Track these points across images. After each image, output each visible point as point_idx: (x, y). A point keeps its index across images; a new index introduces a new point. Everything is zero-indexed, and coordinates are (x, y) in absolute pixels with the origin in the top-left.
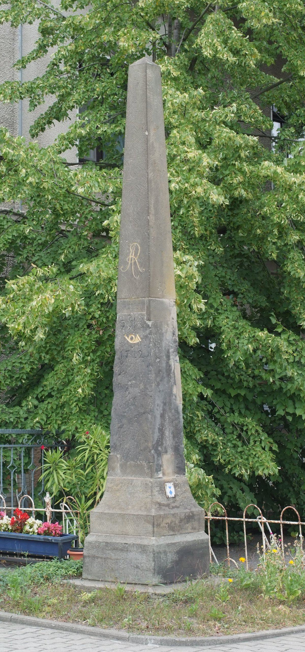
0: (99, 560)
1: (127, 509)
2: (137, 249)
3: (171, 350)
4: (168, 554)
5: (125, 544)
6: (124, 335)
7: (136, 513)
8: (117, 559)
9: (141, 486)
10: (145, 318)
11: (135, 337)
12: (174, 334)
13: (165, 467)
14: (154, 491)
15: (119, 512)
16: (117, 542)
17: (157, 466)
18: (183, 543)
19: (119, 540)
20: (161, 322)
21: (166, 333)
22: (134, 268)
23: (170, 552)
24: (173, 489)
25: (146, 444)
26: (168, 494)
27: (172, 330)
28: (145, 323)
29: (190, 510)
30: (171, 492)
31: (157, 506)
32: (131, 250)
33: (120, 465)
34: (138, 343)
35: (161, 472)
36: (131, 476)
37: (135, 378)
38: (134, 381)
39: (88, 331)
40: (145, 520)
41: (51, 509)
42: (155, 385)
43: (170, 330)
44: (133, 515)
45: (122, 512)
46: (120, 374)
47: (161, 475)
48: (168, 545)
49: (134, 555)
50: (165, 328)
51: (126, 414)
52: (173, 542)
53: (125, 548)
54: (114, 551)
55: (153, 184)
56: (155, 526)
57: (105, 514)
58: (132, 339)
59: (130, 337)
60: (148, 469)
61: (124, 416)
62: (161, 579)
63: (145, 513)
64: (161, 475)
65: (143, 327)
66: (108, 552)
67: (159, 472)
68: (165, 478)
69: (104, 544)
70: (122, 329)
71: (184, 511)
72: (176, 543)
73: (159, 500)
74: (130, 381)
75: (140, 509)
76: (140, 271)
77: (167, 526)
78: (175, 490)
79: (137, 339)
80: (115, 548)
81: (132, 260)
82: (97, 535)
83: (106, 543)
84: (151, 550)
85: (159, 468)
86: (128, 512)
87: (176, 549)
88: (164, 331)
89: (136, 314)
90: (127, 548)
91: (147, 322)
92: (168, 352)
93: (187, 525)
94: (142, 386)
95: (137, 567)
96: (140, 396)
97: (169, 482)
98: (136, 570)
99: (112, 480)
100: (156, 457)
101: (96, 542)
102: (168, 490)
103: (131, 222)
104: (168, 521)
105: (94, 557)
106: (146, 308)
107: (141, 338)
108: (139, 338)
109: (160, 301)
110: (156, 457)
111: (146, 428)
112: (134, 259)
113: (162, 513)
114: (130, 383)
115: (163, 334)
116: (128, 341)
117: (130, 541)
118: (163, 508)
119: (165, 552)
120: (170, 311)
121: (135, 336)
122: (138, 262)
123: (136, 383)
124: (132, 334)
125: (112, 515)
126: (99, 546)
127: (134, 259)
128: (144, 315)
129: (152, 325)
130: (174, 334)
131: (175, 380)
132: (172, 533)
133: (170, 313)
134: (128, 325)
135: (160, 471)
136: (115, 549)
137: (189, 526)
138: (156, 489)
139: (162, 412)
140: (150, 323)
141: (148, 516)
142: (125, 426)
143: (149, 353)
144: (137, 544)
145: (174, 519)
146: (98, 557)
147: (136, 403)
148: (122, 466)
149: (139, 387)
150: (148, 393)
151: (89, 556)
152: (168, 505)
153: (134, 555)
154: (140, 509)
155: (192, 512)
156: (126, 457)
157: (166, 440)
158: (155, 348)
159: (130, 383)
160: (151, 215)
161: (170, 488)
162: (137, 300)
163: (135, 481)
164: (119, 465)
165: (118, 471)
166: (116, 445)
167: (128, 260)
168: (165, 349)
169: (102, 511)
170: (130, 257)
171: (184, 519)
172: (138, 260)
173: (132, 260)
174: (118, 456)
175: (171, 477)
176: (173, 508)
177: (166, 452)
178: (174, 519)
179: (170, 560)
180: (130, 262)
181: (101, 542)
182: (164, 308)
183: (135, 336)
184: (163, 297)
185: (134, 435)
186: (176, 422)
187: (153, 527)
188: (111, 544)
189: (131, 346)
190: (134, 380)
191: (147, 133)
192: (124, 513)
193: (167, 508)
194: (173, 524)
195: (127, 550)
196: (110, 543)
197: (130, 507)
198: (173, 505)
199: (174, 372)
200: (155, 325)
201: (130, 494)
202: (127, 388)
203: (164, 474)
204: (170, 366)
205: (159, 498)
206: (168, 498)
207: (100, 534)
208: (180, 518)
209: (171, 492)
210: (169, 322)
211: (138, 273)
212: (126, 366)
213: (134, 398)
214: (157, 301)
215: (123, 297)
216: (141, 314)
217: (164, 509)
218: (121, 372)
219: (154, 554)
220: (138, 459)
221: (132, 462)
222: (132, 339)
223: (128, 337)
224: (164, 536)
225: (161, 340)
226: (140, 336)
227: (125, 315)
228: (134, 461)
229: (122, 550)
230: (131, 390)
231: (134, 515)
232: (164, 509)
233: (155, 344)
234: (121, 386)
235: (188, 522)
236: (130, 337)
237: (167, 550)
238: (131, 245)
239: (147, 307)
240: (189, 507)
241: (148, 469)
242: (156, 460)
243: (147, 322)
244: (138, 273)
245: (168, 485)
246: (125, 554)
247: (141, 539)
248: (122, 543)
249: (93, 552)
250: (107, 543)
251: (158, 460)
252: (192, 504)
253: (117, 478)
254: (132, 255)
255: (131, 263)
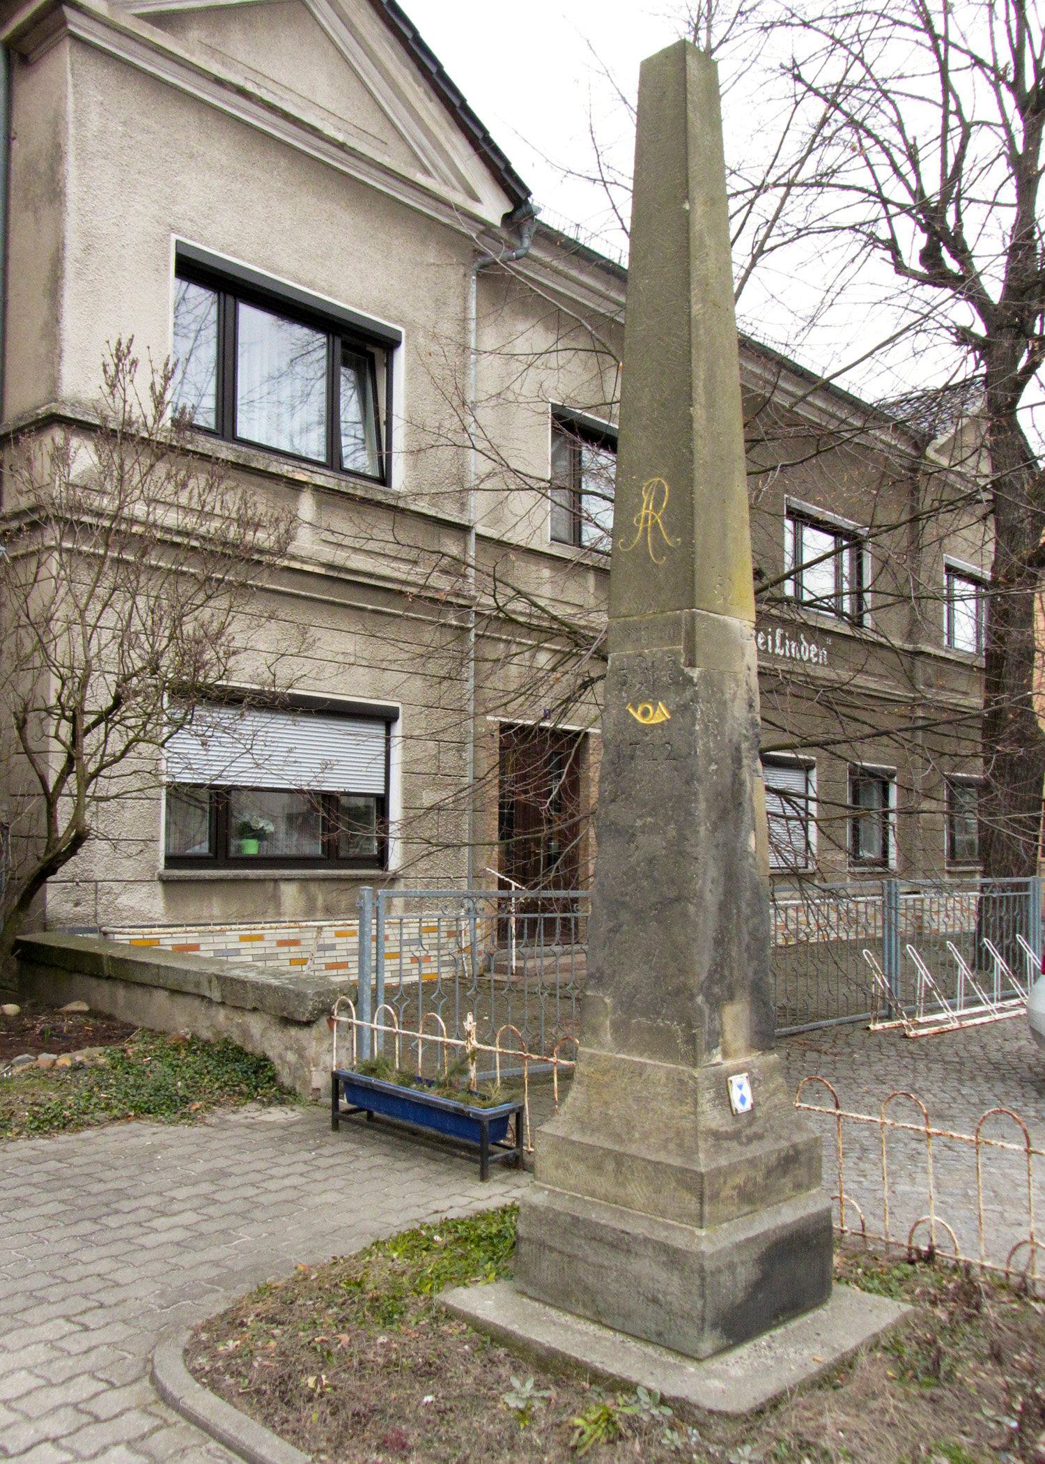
0: (555, 1255)
1: (630, 1140)
2: (660, 491)
3: (745, 745)
4: (739, 1269)
5: (623, 1232)
6: (625, 704)
7: (653, 1158)
8: (601, 1266)
9: (665, 1085)
10: (682, 660)
11: (655, 710)
12: (751, 706)
13: (728, 1036)
14: (701, 1101)
15: (608, 1145)
16: (603, 1222)
17: (709, 1035)
18: (774, 1231)
19: (603, 1217)
20: (722, 673)
21: (733, 701)
22: (654, 539)
23: (743, 1263)
24: (747, 1091)
25: (682, 978)
26: (737, 1104)
27: (746, 696)
28: (682, 673)
29: (789, 1139)
30: (743, 1100)
31: (711, 1141)
32: (645, 498)
33: (613, 1024)
34: (662, 724)
35: (719, 1048)
36: (641, 1055)
37: (653, 812)
38: (649, 819)
39: (661, 1329)
40: (678, 1181)
41: (475, 1043)
42: (707, 829)
43: (742, 693)
44: (644, 1160)
45: (617, 1148)
46: (613, 801)
47: (718, 1058)
48: (739, 1246)
49: (646, 1268)
50: (730, 689)
51: (628, 898)
52: (751, 1234)
53: (621, 1244)
54: (594, 1244)
55: (702, 332)
56: (706, 1199)
57: (573, 1143)
58: (645, 713)
59: (640, 709)
60: (687, 1042)
61: (623, 903)
62: (721, 1338)
63: (677, 1162)
64: (718, 1058)
65: (676, 683)
66: (577, 1241)
67: (714, 1051)
68: (729, 1064)
69: (569, 1219)
70: (621, 690)
71: (776, 1147)
72: (757, 1236)
73: (714, 1125)
74: (640, 817)
75: (665, 1148)
76: (669, 548)
77: (735, 1193)
78: (753, 1089)
79: (660, 714)
80: (596, 1235)
81: (646, 520)
82: (550, 1191)
83: (573, 1217)
84: (696, 1267)
85: (715, 1038)
86: (632, 1149)
87: (756, 1252)
88: (727, 696)
89: (656, 651)
90: (628, 1244)
91: (687, 670)
92: (738, 749)
93: (783, 1181)
94: (672, 831)
95: (655, 1301)
96: (666, 856)
97: (738, 1072)
98: (652, 1307)
99: (592, 1056)
100: (707, 1015)
101: (548, 1209)
102: (735, 1095)
103: (645, 428)
104: (739, 1180)
105: (542, 1245)
106: (683, 634)
107: (671, 713)
108: (665, 712)
109: (718, 621)
110: (707, 1015)
111: (682, 939)
112: (653, 517)
113: (723, 1162)
114: (639, 823)
115: (725, 703)
116: (635, 720)
117: (638, 1228)
118: (726, 1144)
119: (731, 1267)
120: (742, 649)
121: (655, 706)
122: (664, 523)
123: (655, 824)
124: (646, 701)
125: (592, 1148)
126: (555, 1222)
127: (653, 517)
128: (678, 653)
129: (699, 678)
130: (751, 706)
131: (753, 820)
132: (746, 1209)
133: (743, 655)
134: (635, 680)
135: (716, 1047)
136: (594, 1239)
137: (787, 1182)
138: (708, 1096)
139: (722, 897)
140: (695, 673)
141: (687, 1170)
142: (625, 927)
143: (692, 746)
144: (656, 1242)
145: (752, 1173)
146: (551, 1249)
147: (655, 873)
148: (616, 1027)
149: (665, 833)
150: (689, 850)
151: (529, 1239)
152: (735, 1136)
153: (646, 1268)
154: (665, 1148)
155: (794, 1146)
156: (627, 1004)
157: (732, 969)
158: (708, 736)
159: (639, 823)
160: (697, 406)
161: (740, 1087)
162: (659, 616)
163: (649, 1070)
164: (608, 1023)
165: (608, 1037)
166: (602, 973)
167: (638, 522)
168: (730, 741)
169: (562, 1135)
170: (643, 513)
171: (777, 1166)
172: (661, 518)
173: (646, 520)
174: (607, 1000)
175: (741, 1060)
176: (750, 1140)
177: (731, 998)
178: (752, 1173)
179: (741, 1285)
180: (641, 527)
181: (560, 1213)
182: (726, 638)
183: (655, 706)
184: (726, 612)
185: (649, 954)
186: (756, 920)
187: (701, 1203)
188: (588, 1223)
189: (645, 730)
190: (651, 816)
191: (687, 207)
192: (622, 1150)
193: (735, 1144)
194: (750, 1185)
195: (629, 1251)
196: (585, 1220)
197: (637, 1135)
198: (749, 1131)
199: (751, 799)
200: (707, 679)
201: (638, 1100)
202: (633, 835)
203: (726, 1054)
204: (742, 784)
205: (712, 1118)
206: (735, 1115)
207: (558, 1189)
208: (767, 1167)
209: (743, 1100)
210: (740, 676)
211: (661, 548)
212: (632, 779)
213: (651, 861)
214: (713, 619)
215: (623, 610)
216: (670, 651)
217: (728, 1150)
218: (617, 796)
219: (703, 1279)
220: (658, 1013)
221: (643, 1020)
222: (645, 713)
223: (636, 709)
224: (729, 1220)
225: (722, 718)
226: (667, 707)
227: (628, 657)
228: (649, 1018)
229: (614, 1246)
230: (641, 839)
231: (649, 1161)
232: (728, 1150)
233: (707, 727)
234: (617, 831)
235: (785, 1173)
236: (640, 709)
237: (735, 1260)
238: (646, 484)
239: (687, 633)
240: (785, 1133)
241: (687, 1042)
242: (707, 1020)
243: (687, 670)
244: (661, 548)
245: (736, 1080)
246: (622, 1257)
247: (667, 1227)
248: (614, 1229)
249: (541, 1232)
250: (576, 1219)
251: (712, 1020)
252: (791, 1122)
253: (604, 1053)
254: (647, 508)
255: (645, 530)
